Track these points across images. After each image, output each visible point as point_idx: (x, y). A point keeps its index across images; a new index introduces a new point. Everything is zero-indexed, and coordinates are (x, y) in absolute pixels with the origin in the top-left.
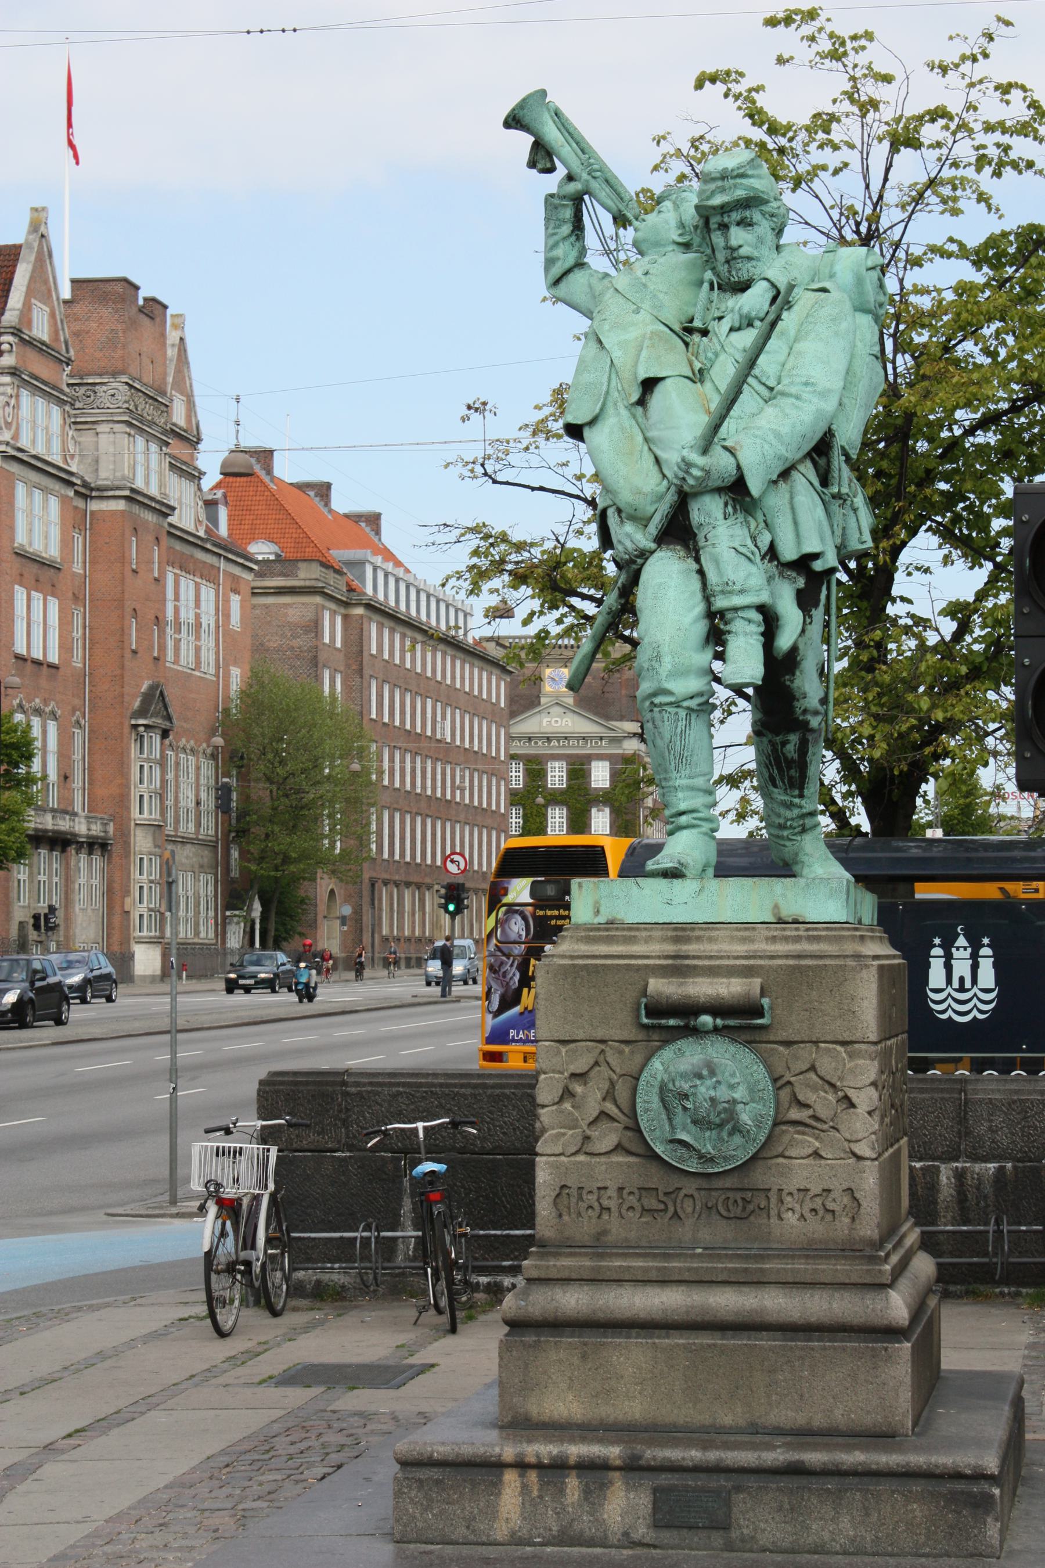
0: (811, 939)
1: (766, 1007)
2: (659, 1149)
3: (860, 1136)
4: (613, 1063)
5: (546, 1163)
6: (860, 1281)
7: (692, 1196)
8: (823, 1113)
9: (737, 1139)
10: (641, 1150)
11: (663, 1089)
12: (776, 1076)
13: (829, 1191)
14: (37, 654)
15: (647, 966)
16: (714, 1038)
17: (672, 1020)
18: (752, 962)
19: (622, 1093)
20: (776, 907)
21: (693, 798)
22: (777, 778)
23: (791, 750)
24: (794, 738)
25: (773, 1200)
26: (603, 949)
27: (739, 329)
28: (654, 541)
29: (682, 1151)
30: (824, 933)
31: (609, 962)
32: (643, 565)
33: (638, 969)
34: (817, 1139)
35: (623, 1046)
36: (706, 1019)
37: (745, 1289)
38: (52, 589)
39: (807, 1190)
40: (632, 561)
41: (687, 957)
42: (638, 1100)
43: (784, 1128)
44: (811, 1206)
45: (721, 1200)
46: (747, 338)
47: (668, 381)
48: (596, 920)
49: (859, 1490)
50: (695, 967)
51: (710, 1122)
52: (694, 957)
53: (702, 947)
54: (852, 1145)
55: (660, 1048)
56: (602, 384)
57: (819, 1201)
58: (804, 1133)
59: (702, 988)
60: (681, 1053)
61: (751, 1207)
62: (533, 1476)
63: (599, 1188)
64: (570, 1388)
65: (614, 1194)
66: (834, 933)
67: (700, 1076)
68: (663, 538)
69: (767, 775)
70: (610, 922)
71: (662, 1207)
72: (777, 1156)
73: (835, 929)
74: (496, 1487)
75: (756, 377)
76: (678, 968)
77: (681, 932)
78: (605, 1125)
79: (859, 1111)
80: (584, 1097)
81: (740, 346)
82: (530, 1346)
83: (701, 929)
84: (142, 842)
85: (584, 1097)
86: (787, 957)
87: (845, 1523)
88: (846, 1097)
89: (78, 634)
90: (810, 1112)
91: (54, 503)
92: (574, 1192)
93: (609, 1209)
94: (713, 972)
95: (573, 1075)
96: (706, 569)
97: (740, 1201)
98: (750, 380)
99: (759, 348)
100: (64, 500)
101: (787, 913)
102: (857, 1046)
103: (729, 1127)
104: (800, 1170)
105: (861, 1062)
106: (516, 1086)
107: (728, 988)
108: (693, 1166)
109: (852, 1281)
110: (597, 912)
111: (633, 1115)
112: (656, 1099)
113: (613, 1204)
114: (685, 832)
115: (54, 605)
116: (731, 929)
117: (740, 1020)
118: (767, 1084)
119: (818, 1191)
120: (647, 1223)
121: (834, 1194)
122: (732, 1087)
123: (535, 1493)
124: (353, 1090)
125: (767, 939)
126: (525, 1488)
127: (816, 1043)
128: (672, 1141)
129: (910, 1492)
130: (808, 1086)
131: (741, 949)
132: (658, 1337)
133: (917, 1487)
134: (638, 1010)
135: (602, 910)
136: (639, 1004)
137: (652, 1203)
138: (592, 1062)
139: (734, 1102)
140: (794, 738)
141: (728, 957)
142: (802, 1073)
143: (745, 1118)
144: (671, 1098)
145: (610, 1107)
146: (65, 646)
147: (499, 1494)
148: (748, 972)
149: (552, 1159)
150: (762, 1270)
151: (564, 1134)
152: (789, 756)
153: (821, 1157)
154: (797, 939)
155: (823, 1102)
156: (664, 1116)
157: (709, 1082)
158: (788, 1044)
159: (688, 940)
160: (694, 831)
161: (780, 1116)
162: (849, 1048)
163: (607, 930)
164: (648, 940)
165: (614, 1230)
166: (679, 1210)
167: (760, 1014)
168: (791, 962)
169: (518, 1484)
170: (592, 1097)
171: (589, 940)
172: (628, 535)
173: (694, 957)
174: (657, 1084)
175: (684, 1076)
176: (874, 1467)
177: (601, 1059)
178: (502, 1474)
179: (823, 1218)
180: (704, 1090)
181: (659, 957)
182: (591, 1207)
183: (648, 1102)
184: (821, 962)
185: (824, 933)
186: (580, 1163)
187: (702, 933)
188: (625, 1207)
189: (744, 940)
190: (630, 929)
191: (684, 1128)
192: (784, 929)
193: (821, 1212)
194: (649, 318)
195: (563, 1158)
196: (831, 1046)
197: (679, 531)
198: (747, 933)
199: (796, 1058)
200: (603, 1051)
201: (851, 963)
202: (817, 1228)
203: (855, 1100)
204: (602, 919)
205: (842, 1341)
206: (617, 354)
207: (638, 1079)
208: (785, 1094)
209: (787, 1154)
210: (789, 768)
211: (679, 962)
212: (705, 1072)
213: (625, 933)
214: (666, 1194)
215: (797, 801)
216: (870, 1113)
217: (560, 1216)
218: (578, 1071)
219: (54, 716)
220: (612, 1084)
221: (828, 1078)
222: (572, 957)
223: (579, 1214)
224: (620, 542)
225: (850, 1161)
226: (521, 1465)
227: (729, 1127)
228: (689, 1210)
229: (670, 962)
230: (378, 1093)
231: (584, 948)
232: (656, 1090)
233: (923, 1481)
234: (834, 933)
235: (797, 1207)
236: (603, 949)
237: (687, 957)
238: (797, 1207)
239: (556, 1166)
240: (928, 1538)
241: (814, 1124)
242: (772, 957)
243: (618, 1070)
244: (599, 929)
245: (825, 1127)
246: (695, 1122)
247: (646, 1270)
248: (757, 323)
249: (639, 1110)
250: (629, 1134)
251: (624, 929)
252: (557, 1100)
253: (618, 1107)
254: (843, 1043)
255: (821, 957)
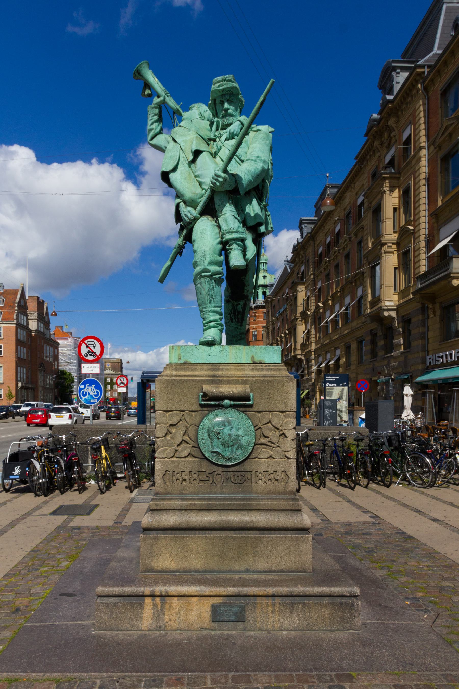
0: (268, 370)
1: (251, 397)
2: (207, 455)
3: (289, 450)
4: (188, 420)
5: (160, 461)
6: (290, 509)
7: (220, 474)
8: (275, 440)
9: (239, 451)
10: (200, 455)
11: (209, 430)
12: (255, 425)
13: (276, 472)
14: (22, 357)
15: (202, 380)
16: (230, 409)
17: (213, 402)
18: (245, 379)
19: (191, 431)
20: (253, 357)
21: (215, 315)
22: (233, 319)
23: (240, 308)
24: (242, 303)
25: (253, 476)
26: (183, 373)
27: (229, 140)
28: (200, 215)
29: (216, 456)
30: (273, 368)
31: (189, 378)
32: (194, 225)
33: (199, 381)
34: (271, 450)
35: (192, 413)
36: (227, 402)
37: (243, 512)
38: (24, 347)
39: (267, 472)
40: (190, 223)
41: (218, 376)
42: (199, 435)
43: (258, 446)
44: (269, 478)
45: (232, 476)
46: (233, 142)
47: (204, 153)
48: (179, 362)
49: (300, 603)
50: (222, 380)
51: (228, 444)
52: (223, 377)
53: (223, 373)
54: (286, 454)
55: (208, 414)
56: (177, 156)
57: (272, 475)
58: (266, 448)
59: (226, 389)
60: (216, 416)
61: (244, 478)
62: (158, 600)
63: (182, 472)
64: (170, 556)
65: (188, 474)
66: (277, 367)
67: (225, 426)
68: (202, 213)
69: (229, 317)
70: (185, 363)
71: (208, 479)
72: (255, 458)
73: (277, 366)
74: (142, 605)
75: (237, 156)
76: (215, 381)
77: (214, 366)
78: (184, 445)
79: (289, 439)
80: (175, 434)
81: (231, 145)
82: (154, 538)
83: (223, 365)
84: (40, 389)
85: (175, 434)
86: (259, 377)
87: (295, 618)
88: (283, 434)
89: (29, 354)
90: (268, 440)
91: (25, 332)
92: (171, 473)
93: (185, 480)
94: (229, 382)
95: (171, 425)
96: (221, 224)
97: (240, 476)
98: (235, 157)
99: (239, 145)
100: (27, 332)
101: (257, 359)
102: (288, 413)
103: (236, 446)
104: (263, 463)
105: (290, 419)
106: (117, 428)
107: (237, 389)
108: (221, 462)
109: (287, 509)
110: (180, 359)
111: (197, 441)
112: (206, 434)
113: (187, 478)
114: (213, 329)
115: (25, 349)
116: (235, 366)
117: (241, 402)
118: (252, 428)
119: (272, 472)
120: (202, 485)
121: (279, 473)
122: (238, 429)
123: (159, 608)
124: (76, 429)
125: (250, 370)
126: (155, 606)
127: (271, 411)
128: (212, 452)
129: (323, 603)
130: (268, 429)
131: (240, 373)
132: (208, 534)
133: (326, 601)
134: (199, 397)
135: (182, 358)
136: (199, 396)
137: (203, 477)
138: (179, 420)
139: (238, 436)
140: (242, 303)
141: (235, 377)
142: (266, 424)
143: (243, 441)
144: (214, 435)
145: (186, 438)
146: (27, 356)
147: (143, 609)
148: (244, 382)
149: (162, 459)
150: (250, 505)
151: (167, 449)
152: (239, 310)
153: (273, 458)
154: (262, 370)
155: (274, 436)
156: (209, 442)
157: (228, 428)
158: (260, 412)
159: (218, 370)
160: (216, 328)
161: (256, 442)
162: (284, 414)
163: (184, 366)
164: (201, 370)
165: (188, 489)
166: (215, 480)
167: (249, 400)
168: (261, 379)
169: (152, 604)
170: (178, 433)
171: (176, 369)
172: (189, 212)
173: (223, 377)
174: (206, 428)
175: (218, 424)
176: (307, 593)
177: (183, 418)
178: (144, 600)
179: (273, 483)
180: (226, 431)
181: (207, 377)
182: (178, 479)
183: (203, 436)
184: (274, 379)
185: (273, 368)
186: (174, 461)
187: (223, 367)
188: (192, 479)
189: (241, 370)
190: (194, 365)
191: (218, 447)
192: (257, 366)
193: (273, 480)
194: (194, 133)
195: (166, 459)
196: (277, 413)
197: (210, 210)
198: (242, 368)
199: (263, 417)
200: (183, 415)
201: (285, 379)
202: (271, 486)
203: (287, 435)
204: (181, 361)
205: (284, 534)
206: (182, 145)
207: (198, 427)
208: (259, 432)
209: (259, 457)
210: (238, 315)
211: (215, 378)
212: (227, 424)
213: (192, 367)
214: (209, 473)
215: (240, 327)
216: (292, 440)
217: (165, 483)
218: (173, 423)
219: (25, 368)
220: (187, 428)
221: (276, 426)
222: (170, 376)
223: (173, 482)
224: (186, 215)
225: (285, 460)
226: (153, 596)
227: (236, 446)
228: (219, 480)
229: (211, 378)
230: (82, 430)
231: (174, 373)
232: (206, 431)
233: (328, 598)
234: (277, 367)
235: (263, 478)
236: (183, 373)
237: (218, 376)
238: (263, 478)
239: (164, 463)
240: (330, 623)
241: (270, 444)
242: (253, 377)
243: (190, 423)
244: (181, 365)
245: (275, 446)
246: (222, 444)
247: (201, 505)
248: (236, 137)
249: (199, 439)
250: (195, 449)
251: (191, 365)
252: (164, 435)
253: (190, 438)
254: (282, 412)
255: (273, 377)
